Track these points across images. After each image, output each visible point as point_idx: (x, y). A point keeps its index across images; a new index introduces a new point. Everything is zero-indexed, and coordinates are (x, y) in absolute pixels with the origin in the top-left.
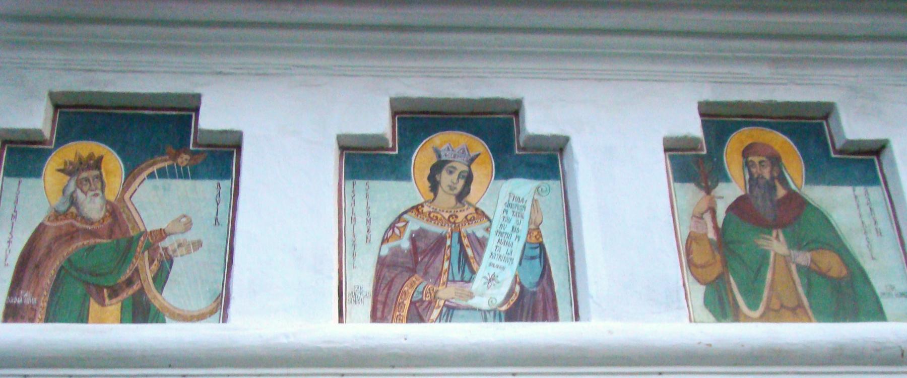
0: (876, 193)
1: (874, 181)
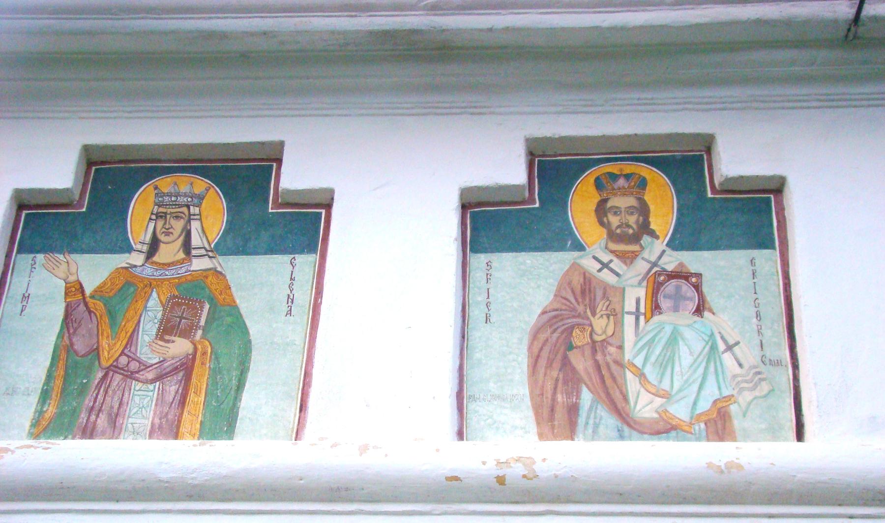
0: (767, 259)
1: (765, 243)
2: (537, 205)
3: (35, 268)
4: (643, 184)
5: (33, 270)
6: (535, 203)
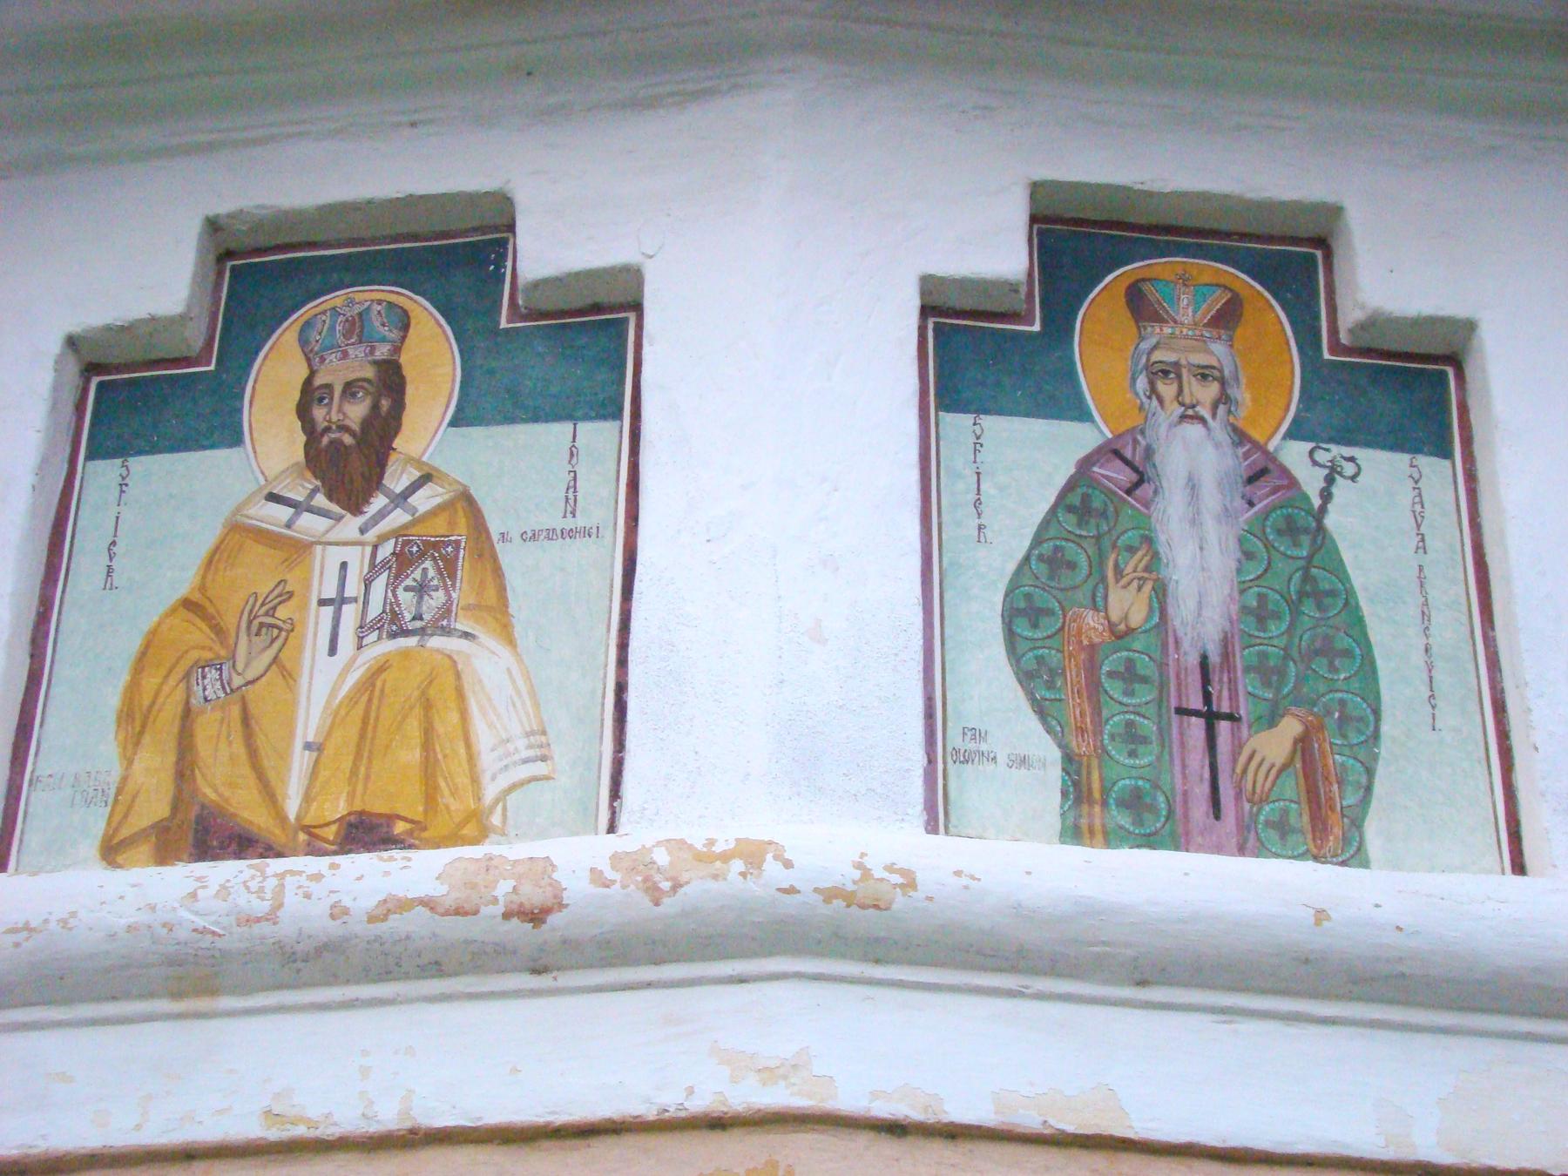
2: (1036, 328)
3: (126, 485)
4: (404, 324)
5: (124, 488)
6: (1032, 324)
